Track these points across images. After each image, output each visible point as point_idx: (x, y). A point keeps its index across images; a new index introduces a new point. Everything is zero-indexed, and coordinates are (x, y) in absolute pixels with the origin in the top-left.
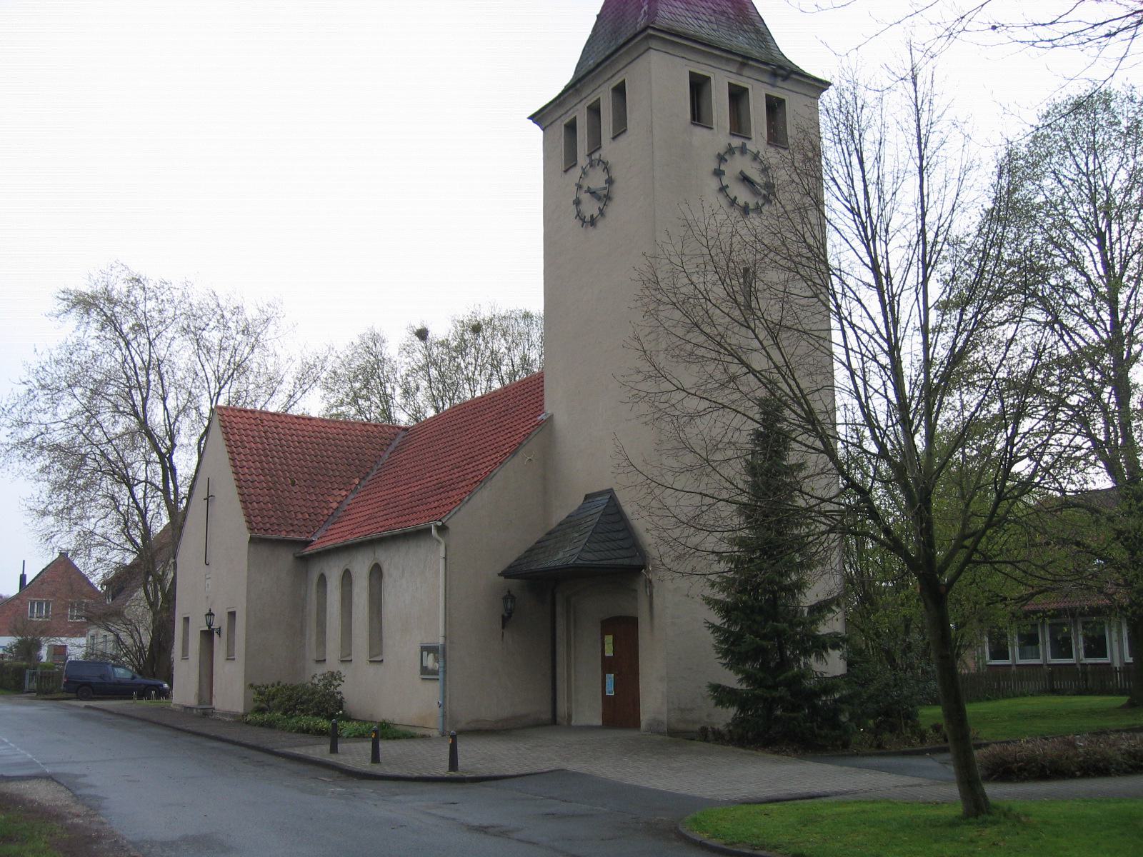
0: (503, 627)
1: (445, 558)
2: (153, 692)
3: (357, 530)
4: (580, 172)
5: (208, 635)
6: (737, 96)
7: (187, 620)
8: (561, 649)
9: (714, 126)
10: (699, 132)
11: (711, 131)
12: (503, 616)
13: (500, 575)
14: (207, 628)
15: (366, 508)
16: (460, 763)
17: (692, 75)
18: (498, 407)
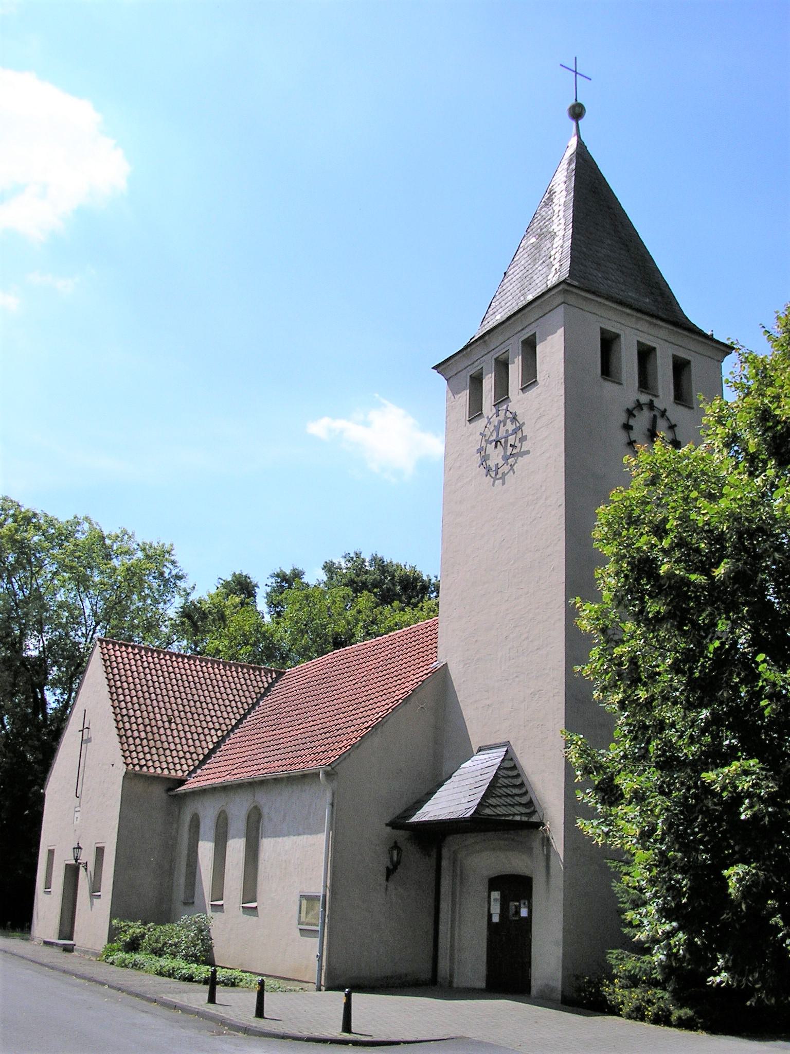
0: (387, 880)
1: (332, 805)
2: (9, 923)
3: (236, 771)
4: (486, 420)
5: (72, 872)
6: (645, 354)
7: (51, 853)
8: (445, 906)
9: (624, 382)
10: (609, 386)
11: (620, 387)
12: (387, 868)
13: (387, 825)
14: (74, 862)
15: (244, 749)
16: (354, 1026)
17: (603, 332)
18: (383, 654)
